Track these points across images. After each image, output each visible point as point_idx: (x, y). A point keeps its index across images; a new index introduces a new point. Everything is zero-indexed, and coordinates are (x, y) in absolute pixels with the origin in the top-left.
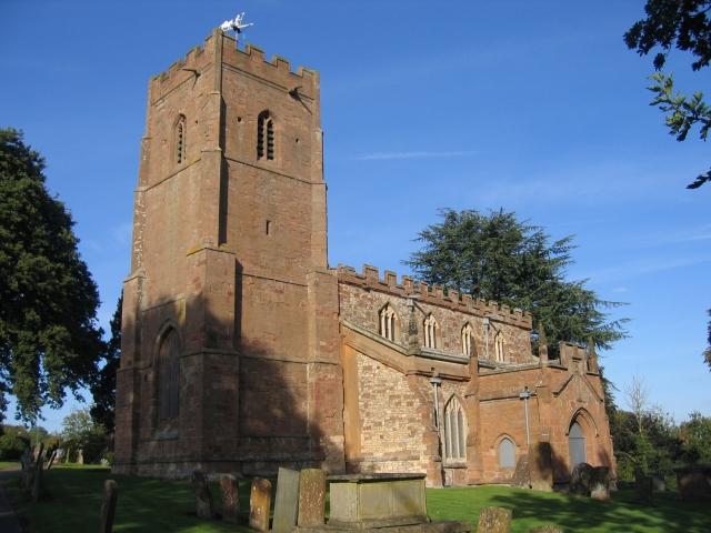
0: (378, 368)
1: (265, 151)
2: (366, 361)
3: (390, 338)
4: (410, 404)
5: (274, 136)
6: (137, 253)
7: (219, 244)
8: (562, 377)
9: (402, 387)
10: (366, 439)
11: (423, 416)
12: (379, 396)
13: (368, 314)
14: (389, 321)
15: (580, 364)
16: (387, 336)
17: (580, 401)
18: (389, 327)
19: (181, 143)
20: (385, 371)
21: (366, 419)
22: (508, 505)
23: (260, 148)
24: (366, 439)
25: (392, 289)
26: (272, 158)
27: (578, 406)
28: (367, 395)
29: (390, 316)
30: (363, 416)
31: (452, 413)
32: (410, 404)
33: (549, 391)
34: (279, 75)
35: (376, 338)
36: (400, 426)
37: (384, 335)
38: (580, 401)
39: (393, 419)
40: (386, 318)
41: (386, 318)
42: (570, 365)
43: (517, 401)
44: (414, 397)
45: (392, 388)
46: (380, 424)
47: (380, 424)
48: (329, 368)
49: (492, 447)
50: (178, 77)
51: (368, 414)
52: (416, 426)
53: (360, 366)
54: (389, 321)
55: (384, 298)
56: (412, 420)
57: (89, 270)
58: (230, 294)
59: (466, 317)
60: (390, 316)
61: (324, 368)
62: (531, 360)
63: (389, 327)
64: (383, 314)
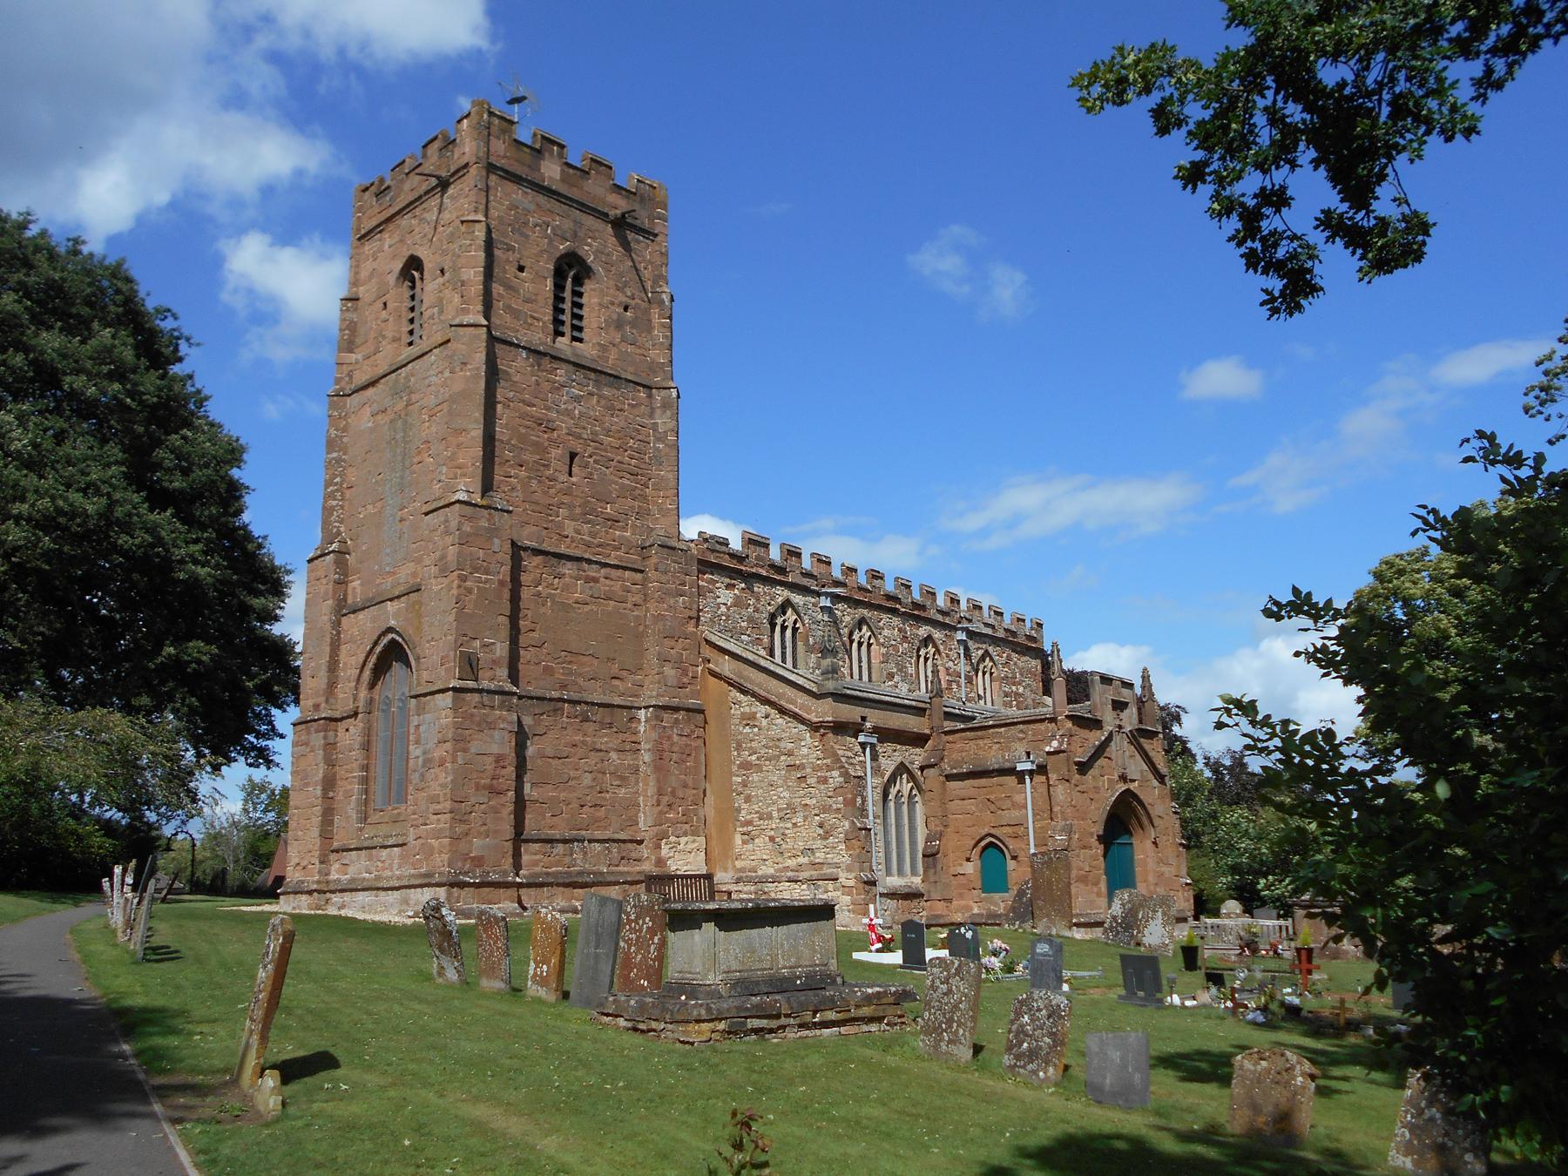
0: (767, 717)
1: (567, 329)
2: (746, 704)
3: (789, 665)
4: (824, 781)
5: (584, 300)
6: (332, 509)
7: (484, 493)
8: (1096, 737)
9: (808, 747)
10: (744, 842)
11: (846, 803)
12: (767, 766)
13: (751, 620)
14: (789, 633)
15: (1125, 714)
16: (784, 660)
17: (1123, 778)
18: (789, 644)
19: (413, 297)
20: (780, 721)
21: (744, 806)
22: (1221, 1139)
23: (558, 322)
24: (744, 842)
25: (933, 614)
26: (580, 340)
27: (1122, 787)
28: (746, 766)
29: (789, 624)
30: (739, 802)
31: (899, 795)
32: (824, 781)
33: (1068, 759)
34: (594, 189)
35: (763, 663)
36: (805, 818)
37: (778, 659)
38: (1123, 778)
39: (791, 808)
40: (784, 628)
41: (784, 628)
42: (1109, 718)
43: (1011, 781)
44: (829, 768)
45: (790, 754)
46: (770, 817)
47: (770, 817)
48: (681, 715)
49: (968, 860)
50: (407, 186)
51: (748, 799)
52: (830, 818)
53: (736, 711)
54: (789, 633)
55: (782, 594)
56: (826, 809)
57: (1399, 272)
58: (501, 583)
59: (923, 631)
60: (789, 624)
61: (668, 717)
62: (1037, 704)
63: (789, 644)
64: (779, 621)
